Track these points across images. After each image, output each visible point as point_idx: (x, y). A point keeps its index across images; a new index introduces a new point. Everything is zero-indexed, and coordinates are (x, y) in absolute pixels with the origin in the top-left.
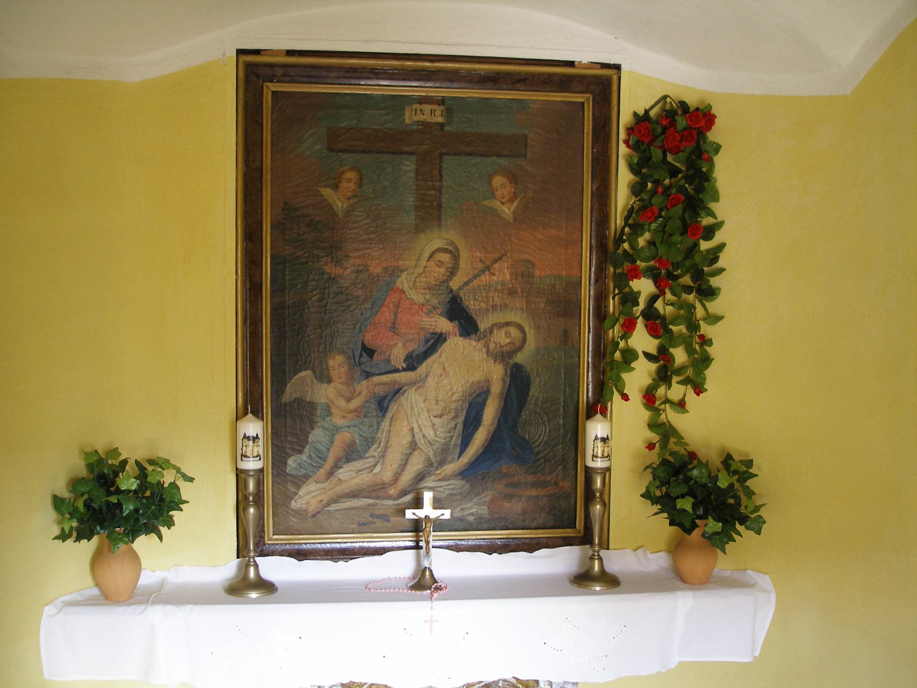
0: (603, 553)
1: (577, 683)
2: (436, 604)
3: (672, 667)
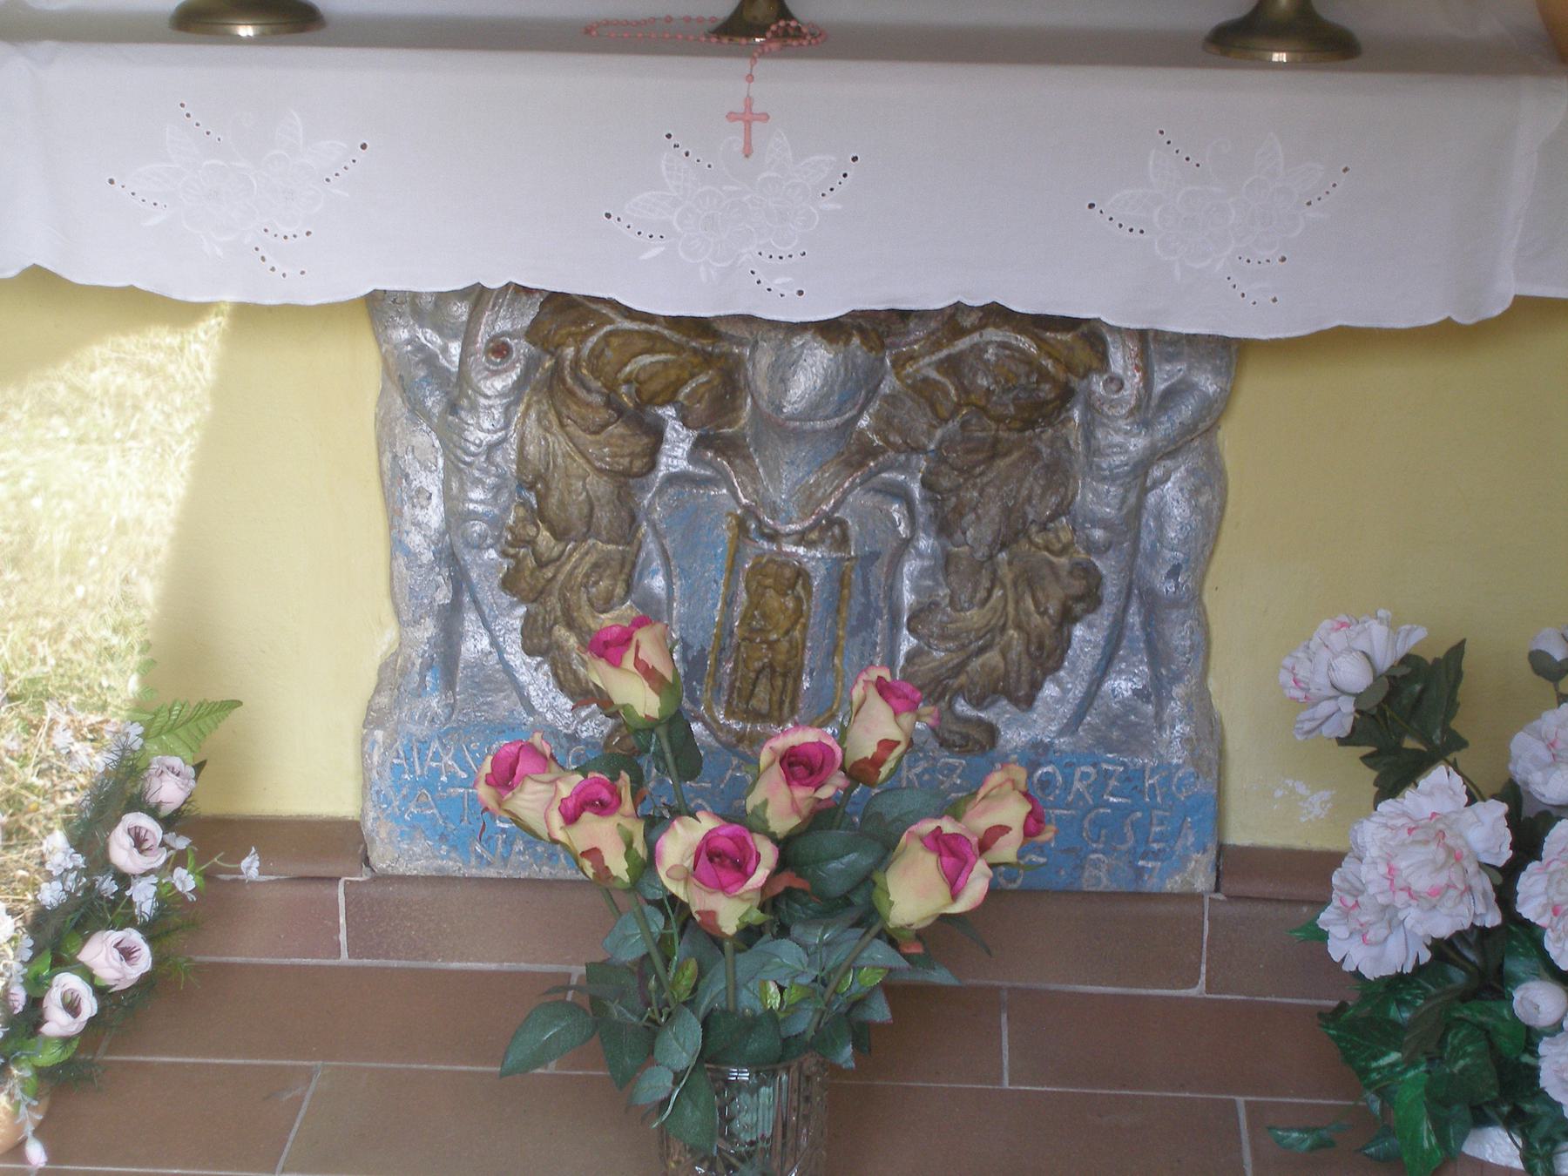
2: (764, 66)
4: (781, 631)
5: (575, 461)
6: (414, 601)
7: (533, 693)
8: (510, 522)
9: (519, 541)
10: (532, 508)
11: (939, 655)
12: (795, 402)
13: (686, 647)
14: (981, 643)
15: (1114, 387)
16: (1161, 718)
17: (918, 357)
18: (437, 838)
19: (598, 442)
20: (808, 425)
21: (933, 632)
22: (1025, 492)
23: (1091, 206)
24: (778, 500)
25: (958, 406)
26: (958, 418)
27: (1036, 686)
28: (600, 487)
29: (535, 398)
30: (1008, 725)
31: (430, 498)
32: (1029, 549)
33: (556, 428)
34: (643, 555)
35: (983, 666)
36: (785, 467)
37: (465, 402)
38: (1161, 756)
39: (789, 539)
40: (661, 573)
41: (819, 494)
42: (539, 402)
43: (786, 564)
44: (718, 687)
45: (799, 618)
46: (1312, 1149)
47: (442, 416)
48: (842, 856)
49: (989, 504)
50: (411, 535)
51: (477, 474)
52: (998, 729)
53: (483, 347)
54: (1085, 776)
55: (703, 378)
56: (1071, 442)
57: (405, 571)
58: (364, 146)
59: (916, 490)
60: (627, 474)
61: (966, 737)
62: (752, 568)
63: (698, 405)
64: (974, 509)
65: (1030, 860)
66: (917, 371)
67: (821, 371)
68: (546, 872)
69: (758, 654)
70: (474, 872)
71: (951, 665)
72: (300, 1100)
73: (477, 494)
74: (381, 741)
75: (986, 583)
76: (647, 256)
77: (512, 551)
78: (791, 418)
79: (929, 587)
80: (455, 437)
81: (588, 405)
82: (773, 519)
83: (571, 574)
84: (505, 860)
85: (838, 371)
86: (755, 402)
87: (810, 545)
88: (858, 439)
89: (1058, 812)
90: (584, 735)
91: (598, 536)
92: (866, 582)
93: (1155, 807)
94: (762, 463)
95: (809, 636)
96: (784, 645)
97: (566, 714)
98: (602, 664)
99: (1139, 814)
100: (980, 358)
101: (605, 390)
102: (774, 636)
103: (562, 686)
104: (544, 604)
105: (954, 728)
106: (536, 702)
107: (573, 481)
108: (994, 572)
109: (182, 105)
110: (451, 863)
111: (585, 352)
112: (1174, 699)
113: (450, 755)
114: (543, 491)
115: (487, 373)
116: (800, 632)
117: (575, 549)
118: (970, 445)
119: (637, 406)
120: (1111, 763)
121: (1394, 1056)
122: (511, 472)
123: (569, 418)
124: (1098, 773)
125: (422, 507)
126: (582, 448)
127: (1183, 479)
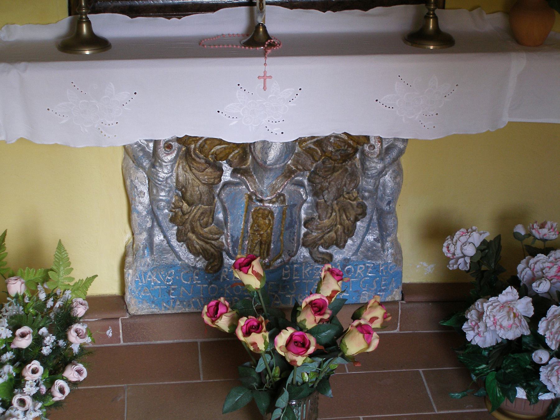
0: (438, 12)
1: (407, 140)
2: (269, 60)
3: (502, 126)
4: (264, 231)
5: (195, 181)
6: (140, 227)
7: (181, 254)
8: (173, 201)
9: (176, 207)
10: (180, 196)
11: (314, 234)
12: (271, 160)
13: (232, 237)
14: (329, 230)
15: (372, 148)
16: (384, 248)
17: (307, 141)
18: (151, 302)
19: (203, 175)
20: (274, 167)
21: (313, 228)
22: (343, 183)
23: (377, 100)
24: (263, 190)
25: (322, 156)
26: (321, 160)
27: (346, 241)
28: (203, 189)
29: (181, 161)
30: (336, 253)
31: (144, 194)
32: (343, 199)
33: (189, 171)
34: (216, 208)
35: (329, 237)
36: (265, 179)
37: (158, 164)
38: (385, 260)
39: (267, 202)
40: (221, 213)
41: (277, 187)
42: (182, 162)
43: (265, 209)
44: (243, 249)
45: (270, 226)
46: (461, 397)
47: (149, 168)
48: (326, 331)
49: (332, 187)
50: (139, 207)
51: (163, 187)
52: (333, 255)
53: (163, 145)
54: (361, 268)
55: (236, 151)
56: (357, 165)
57: (137, 218)
58: (135, 93)
59: (306, 182)
60: (213, 184)
61: (323, 259)
62: (254, 211)
63: (235, 160)
64: (327, 189)
65: (344, 295)
66: (307, 145)
67: (279, 149)
68: (187, 310)
69: (256, 238)
70: (164, 312)
71: (319, 237)
72: (123, 401)
73: (163, 194)
74: (131, 273)
75: (330, 211)
76: (232, 124)
77: (174, 210)
78: (270, 165)
79: (310, 213)
80: (155, 176)
81: (200, 163)
82: (262, 196)
83: (194, 217)
84: (173, 307)
85: (284, 149)
86: (254, 158)
87: (274, 203)
88: (288, 168)
89: (352, 280)
90: (198, 266)
91: (203, 204)
92: (291, 213)
93: (384, 276)
94: (256, 177)
95: (273, 231)
96: (265, 235)
97: (192, 260)
98: (241, 273)
99: (378, 279)
100: (329, 141)
101: (205, 158)
102: (262, 232)
103: (190, 251)
104: (185, 226)
105: (319, 256)
106: (182, 257)
107: (195, 188)
108: (332, 207)
109: (72, 83)
110: (156, 310)
111: (198, 145)
112: (388, 242)
113: (155, 276)
114: (184, 191)
115: (165, 154)
116: (270, 230)
117: (195, 208)
118: (326, 169)
119: (214, 161)
120: (369, 263)
121: (484, 366)
122: (174, 186)
123: (193, 167)
124: (365, 267)
125: (142, 197)
126: (198, 177)
127: (391, 174)
